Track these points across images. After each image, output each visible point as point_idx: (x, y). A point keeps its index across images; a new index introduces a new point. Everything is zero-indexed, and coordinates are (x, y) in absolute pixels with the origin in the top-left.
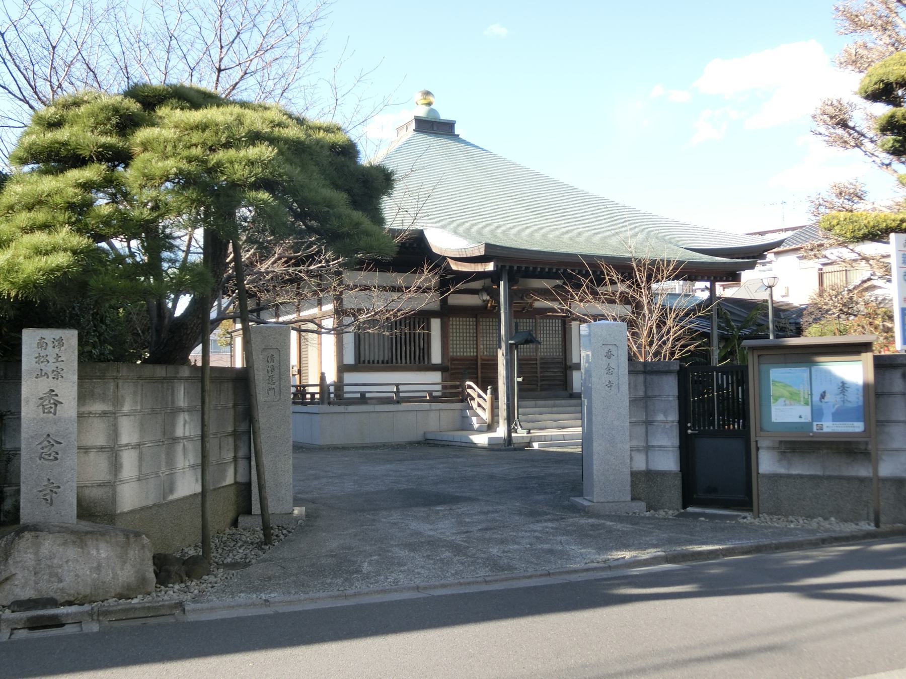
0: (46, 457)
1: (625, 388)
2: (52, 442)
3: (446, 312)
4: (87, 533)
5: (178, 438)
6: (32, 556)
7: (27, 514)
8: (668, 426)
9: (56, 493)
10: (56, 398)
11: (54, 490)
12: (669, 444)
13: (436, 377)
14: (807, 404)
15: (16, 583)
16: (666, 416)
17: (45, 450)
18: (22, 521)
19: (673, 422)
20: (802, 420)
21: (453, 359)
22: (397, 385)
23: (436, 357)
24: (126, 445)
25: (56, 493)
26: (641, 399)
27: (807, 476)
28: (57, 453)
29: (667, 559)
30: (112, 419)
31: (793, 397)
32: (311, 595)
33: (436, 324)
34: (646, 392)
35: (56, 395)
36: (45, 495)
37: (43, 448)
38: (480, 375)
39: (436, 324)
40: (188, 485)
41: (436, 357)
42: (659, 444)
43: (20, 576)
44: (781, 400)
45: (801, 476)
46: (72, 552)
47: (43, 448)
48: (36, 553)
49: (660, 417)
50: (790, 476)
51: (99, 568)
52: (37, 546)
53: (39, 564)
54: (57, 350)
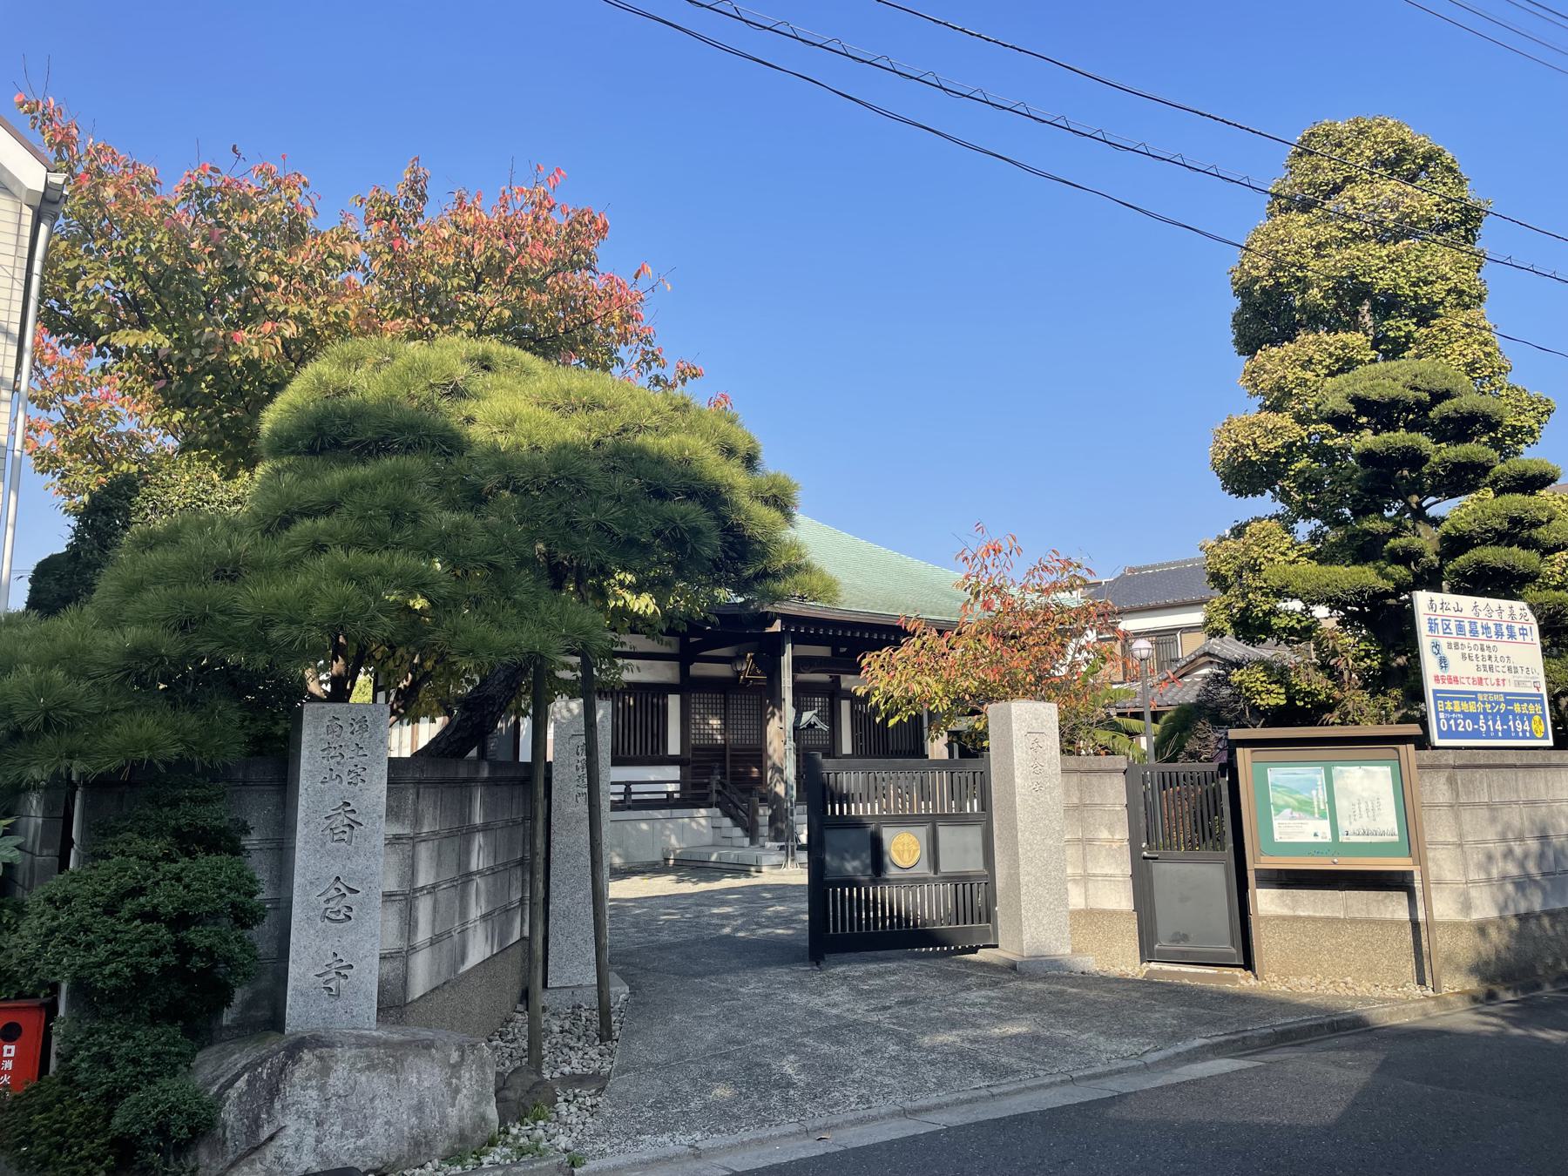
0: (333, 916)
1: (1058, 793)
2: (344, 890)
3: (687, 687)
4: (402, 1044)
5: (472, 874)
6: (314, 1093)
7: (299, 1014)
8: (1115, 846)
9: (346, 977)
10: (352, 816)
11: (343, 972)
12: (1118, 872)
13: (674, 772)
14: (1323, 817)
15: (285, 1142)
16: (1113, 834)
17: (331, 904)
18: (288, 1030)
19: (1122, 840)
20: (1319, 840)
21: (696, 748)
22: (628, 784)
23: (674, 748)
24: (422, 888)
25: (346, 977)
26: (1076, 807)
27: (1321, 919)
28: (350, 909)
29: (1216, 1050)
30: (408, 848)
31: (1305, 808)
32: (744, 1135)
33: (674, 702)
34: (1080, 799)
35: (353, 811)
36: (327, 982)
37: (328, 901)
38: (728, 769)
39: (674, 702)
40: (478, 950)
41: (674, 748)
42: (1105, 871)
43: (290, 1131)
44: (1287, 811)
45: (1314, 919)
46: (377, 1083)
47: (328, 901)
48: (322, 1088)
49: (1105, 834)
50: (1297, 918)
51: (419, 1108)
52: (325, 1071)
53: (328, 1106)
54: (356, 738)
